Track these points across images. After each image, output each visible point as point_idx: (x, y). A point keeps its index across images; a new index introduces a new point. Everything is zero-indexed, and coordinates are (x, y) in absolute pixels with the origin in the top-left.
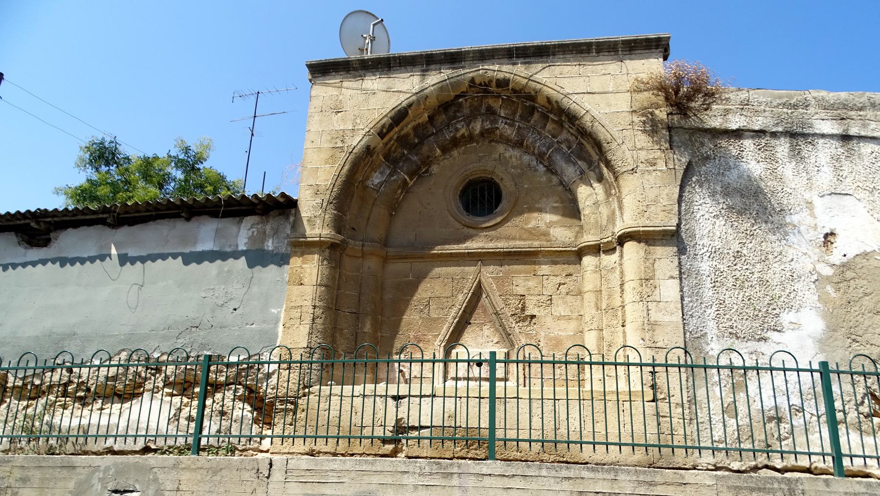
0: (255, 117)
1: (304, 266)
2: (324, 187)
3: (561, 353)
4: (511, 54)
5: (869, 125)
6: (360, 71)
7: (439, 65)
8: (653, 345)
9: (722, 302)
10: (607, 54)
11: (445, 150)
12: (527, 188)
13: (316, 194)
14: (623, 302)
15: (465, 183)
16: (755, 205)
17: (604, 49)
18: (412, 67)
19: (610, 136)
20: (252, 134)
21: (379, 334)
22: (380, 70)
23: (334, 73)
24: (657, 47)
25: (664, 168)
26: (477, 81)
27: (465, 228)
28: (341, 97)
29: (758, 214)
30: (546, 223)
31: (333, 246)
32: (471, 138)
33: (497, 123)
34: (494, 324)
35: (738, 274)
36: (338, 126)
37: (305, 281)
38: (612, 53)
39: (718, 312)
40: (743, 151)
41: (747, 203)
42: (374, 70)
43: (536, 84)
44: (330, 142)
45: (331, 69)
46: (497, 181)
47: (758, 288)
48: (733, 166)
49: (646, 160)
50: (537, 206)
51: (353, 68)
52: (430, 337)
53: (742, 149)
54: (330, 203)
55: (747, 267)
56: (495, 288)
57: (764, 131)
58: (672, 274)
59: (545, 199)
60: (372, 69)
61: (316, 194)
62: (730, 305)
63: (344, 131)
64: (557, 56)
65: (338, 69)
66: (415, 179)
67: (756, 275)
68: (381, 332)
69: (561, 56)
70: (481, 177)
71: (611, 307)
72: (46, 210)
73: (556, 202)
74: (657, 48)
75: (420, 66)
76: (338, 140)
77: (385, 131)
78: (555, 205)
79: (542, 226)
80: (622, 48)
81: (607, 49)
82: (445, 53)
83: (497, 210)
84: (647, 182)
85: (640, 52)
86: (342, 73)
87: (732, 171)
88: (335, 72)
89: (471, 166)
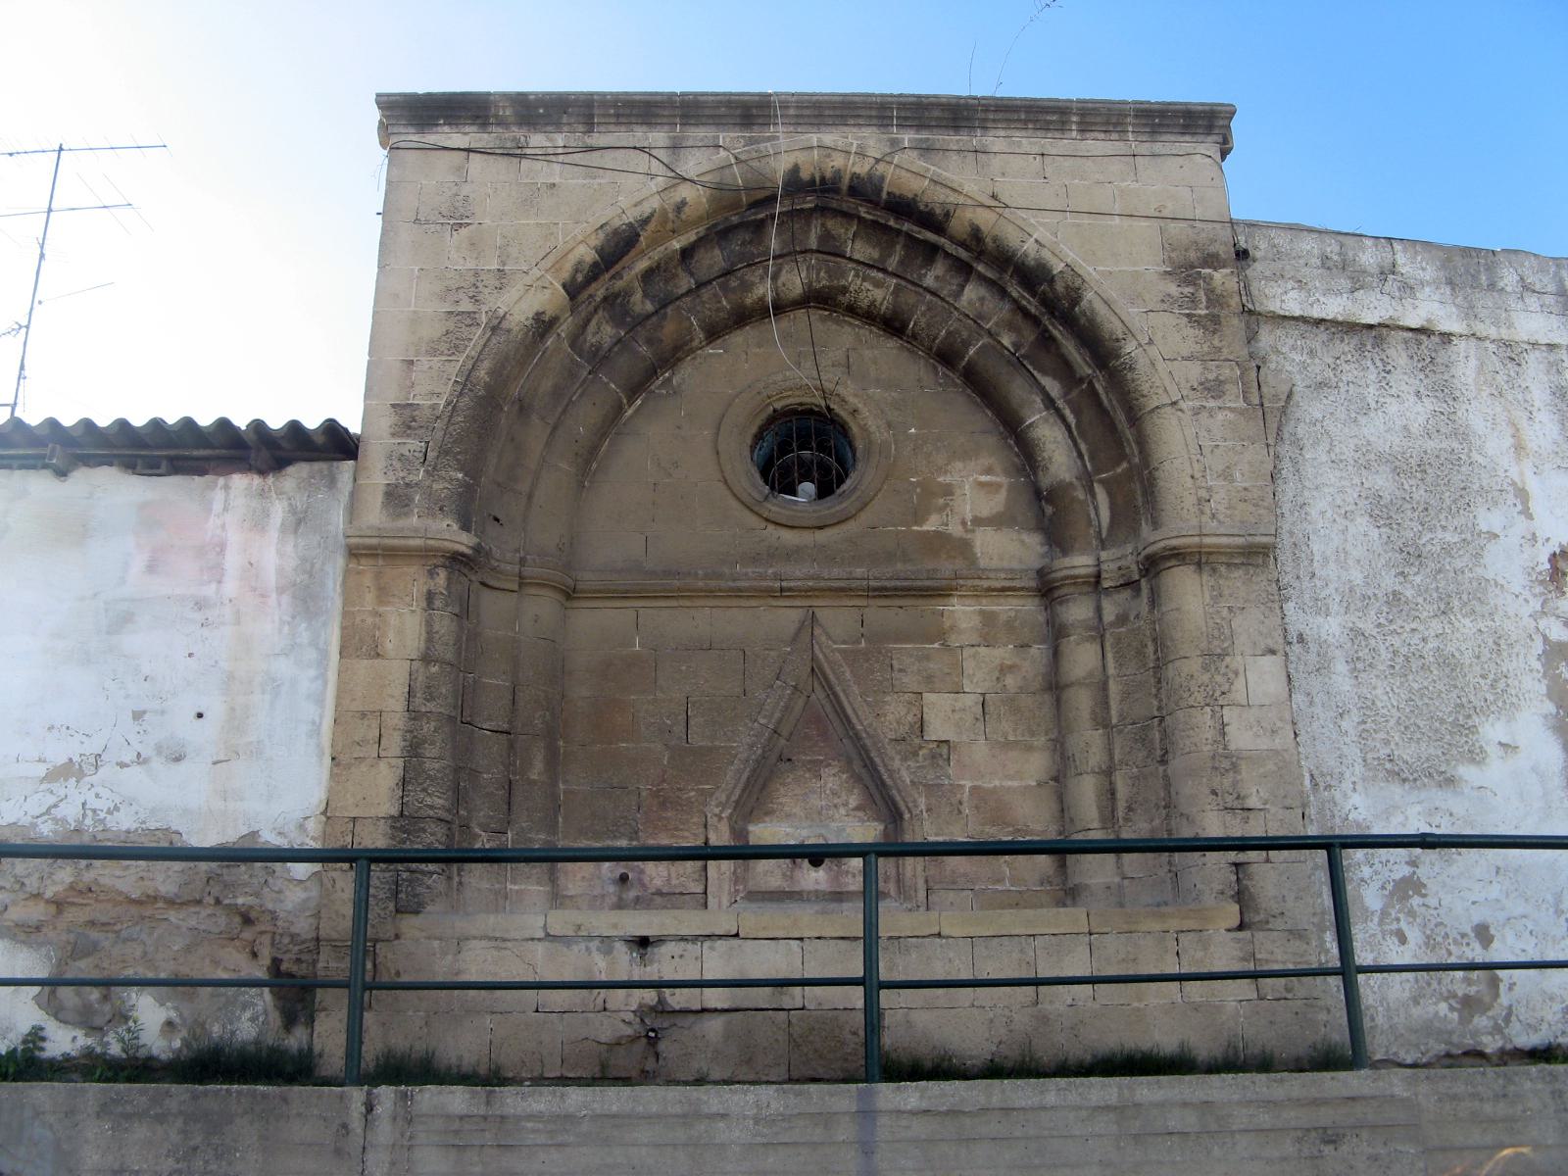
0: (50, 210)
1: (381, 609)
2: (428, 412)
3: (1011, 829)
4: (884, 117)
5: (666, 313)
6: (514, 128)
7: (713, 128)
8: (1236, 804)
9: (1369, 704)
10: (1102, 136)
11: (714, 333)
12: (916, 435)
13: (409, 428)
14: (1160, 708)
15: (764, 416)
16: (1422, 492)
17: (1095, 124)
18: (644, 128)
19: (1121, 325)
20: (42, 256)
21: (561, 786)
22: (565, 129)
23: (446, 129)
24: (1209, 129)
25: (1241, 404)
26: (805, 175)
27: (771, 527)
28: (466, 190)
29: (1426, 509)
30: (964, 523)
31: (457, 561)
32: (781, 307)
33: (843, 274)
34: (849, 762)
35: (1397, 641)
36: (462, 261)
37: (389, 645)
38: (1115, 136)
39: (1363, 726)
40: (1389, 372)
41: (1406, 487)
42: (549, 128)
43: (948, 191)
44: (443, 299)
45: (438, 118)
46: (843, 413)
47: (1435, 672)
48: (1373, 405)
49: (1201, 384)
50: (940, 479)
51: (496, 116)
52: (692, 794)
53: (1389, 368)
54: (444, 452)
55: (1413, 626)
56: (848, 675)
57: (1427, 329)
58: (1270, 643)
59: (959, 465)
60: (547, 124)
61: (409, 428)
62: (1385, 711)
63: (476, 274)
64: (992, 133)
65: (460, 117)
66: (639, 402)
67: (1432, 644)
68: (565, 782)
69: (1002, 133)
70: (801, 404)
71: (1128, 721)
72: (188, 424)
73: (989, 471)
74: (1209, 134)
75: (666, 128)
76: (461, 295)
77: (580, 278)
78: (983, 478)
79: (955, 529)
80: (1134, 125)
81: (1103, 124)
82: (729, 102)
83: (844, 487)
84: (1205, 434)
85: (1172, 138)
86: (467, 129)
87: (1372, 414)
88: (450, 124)
89: (780, 377)
